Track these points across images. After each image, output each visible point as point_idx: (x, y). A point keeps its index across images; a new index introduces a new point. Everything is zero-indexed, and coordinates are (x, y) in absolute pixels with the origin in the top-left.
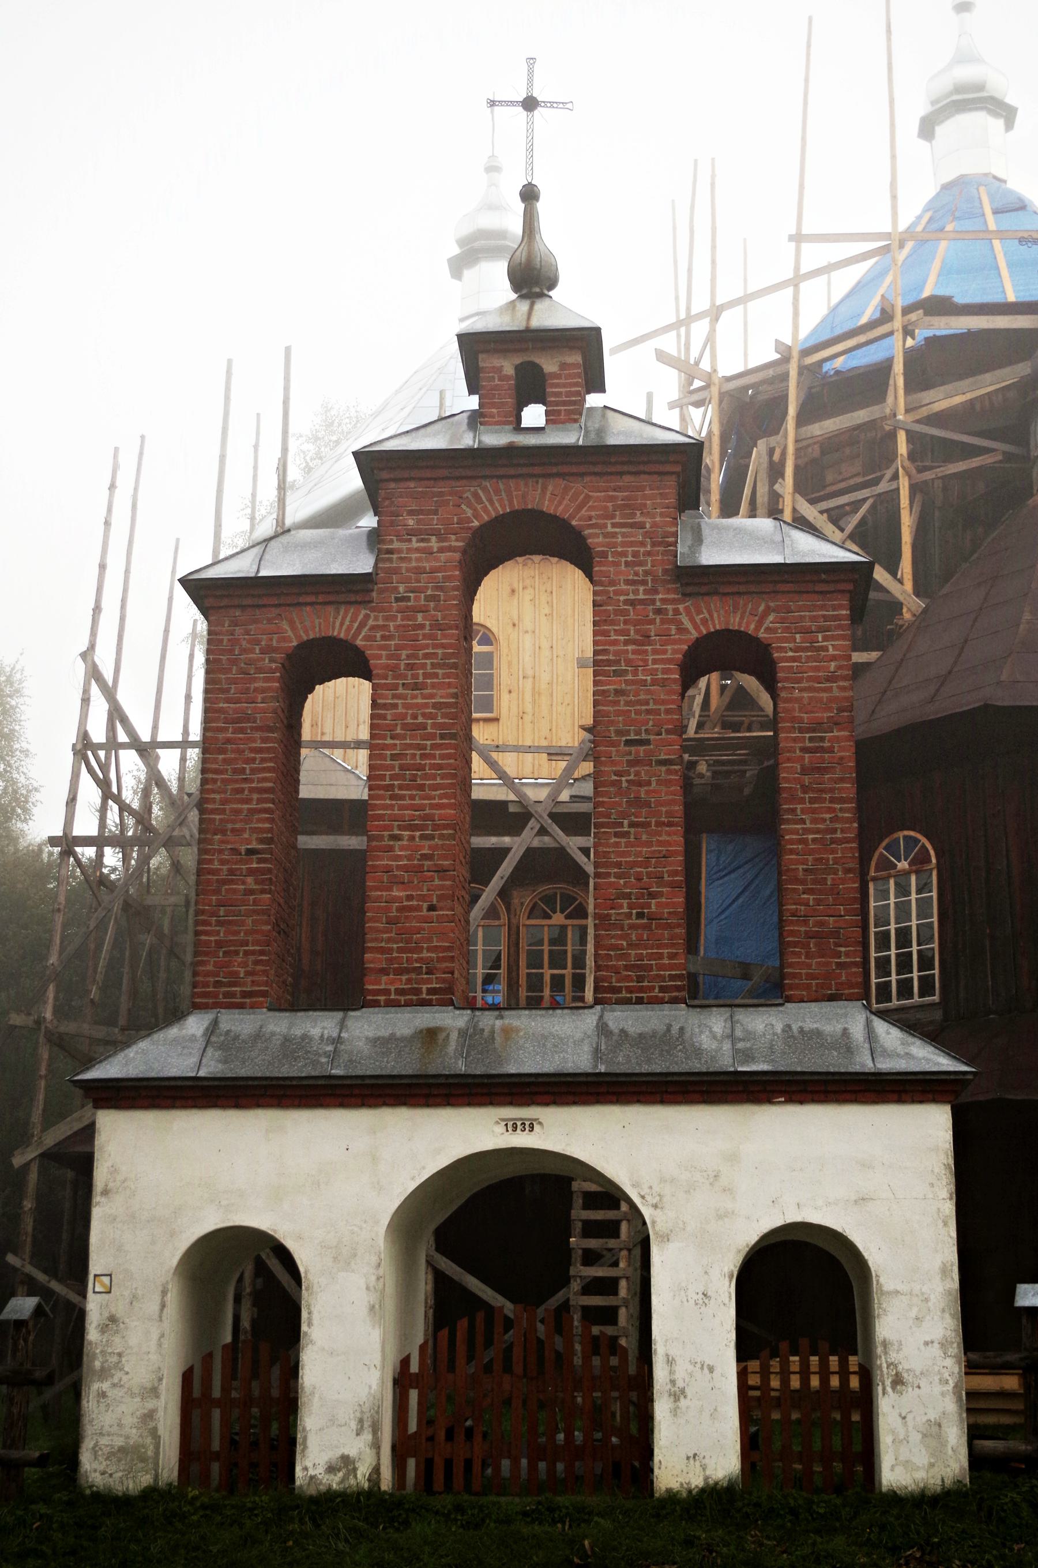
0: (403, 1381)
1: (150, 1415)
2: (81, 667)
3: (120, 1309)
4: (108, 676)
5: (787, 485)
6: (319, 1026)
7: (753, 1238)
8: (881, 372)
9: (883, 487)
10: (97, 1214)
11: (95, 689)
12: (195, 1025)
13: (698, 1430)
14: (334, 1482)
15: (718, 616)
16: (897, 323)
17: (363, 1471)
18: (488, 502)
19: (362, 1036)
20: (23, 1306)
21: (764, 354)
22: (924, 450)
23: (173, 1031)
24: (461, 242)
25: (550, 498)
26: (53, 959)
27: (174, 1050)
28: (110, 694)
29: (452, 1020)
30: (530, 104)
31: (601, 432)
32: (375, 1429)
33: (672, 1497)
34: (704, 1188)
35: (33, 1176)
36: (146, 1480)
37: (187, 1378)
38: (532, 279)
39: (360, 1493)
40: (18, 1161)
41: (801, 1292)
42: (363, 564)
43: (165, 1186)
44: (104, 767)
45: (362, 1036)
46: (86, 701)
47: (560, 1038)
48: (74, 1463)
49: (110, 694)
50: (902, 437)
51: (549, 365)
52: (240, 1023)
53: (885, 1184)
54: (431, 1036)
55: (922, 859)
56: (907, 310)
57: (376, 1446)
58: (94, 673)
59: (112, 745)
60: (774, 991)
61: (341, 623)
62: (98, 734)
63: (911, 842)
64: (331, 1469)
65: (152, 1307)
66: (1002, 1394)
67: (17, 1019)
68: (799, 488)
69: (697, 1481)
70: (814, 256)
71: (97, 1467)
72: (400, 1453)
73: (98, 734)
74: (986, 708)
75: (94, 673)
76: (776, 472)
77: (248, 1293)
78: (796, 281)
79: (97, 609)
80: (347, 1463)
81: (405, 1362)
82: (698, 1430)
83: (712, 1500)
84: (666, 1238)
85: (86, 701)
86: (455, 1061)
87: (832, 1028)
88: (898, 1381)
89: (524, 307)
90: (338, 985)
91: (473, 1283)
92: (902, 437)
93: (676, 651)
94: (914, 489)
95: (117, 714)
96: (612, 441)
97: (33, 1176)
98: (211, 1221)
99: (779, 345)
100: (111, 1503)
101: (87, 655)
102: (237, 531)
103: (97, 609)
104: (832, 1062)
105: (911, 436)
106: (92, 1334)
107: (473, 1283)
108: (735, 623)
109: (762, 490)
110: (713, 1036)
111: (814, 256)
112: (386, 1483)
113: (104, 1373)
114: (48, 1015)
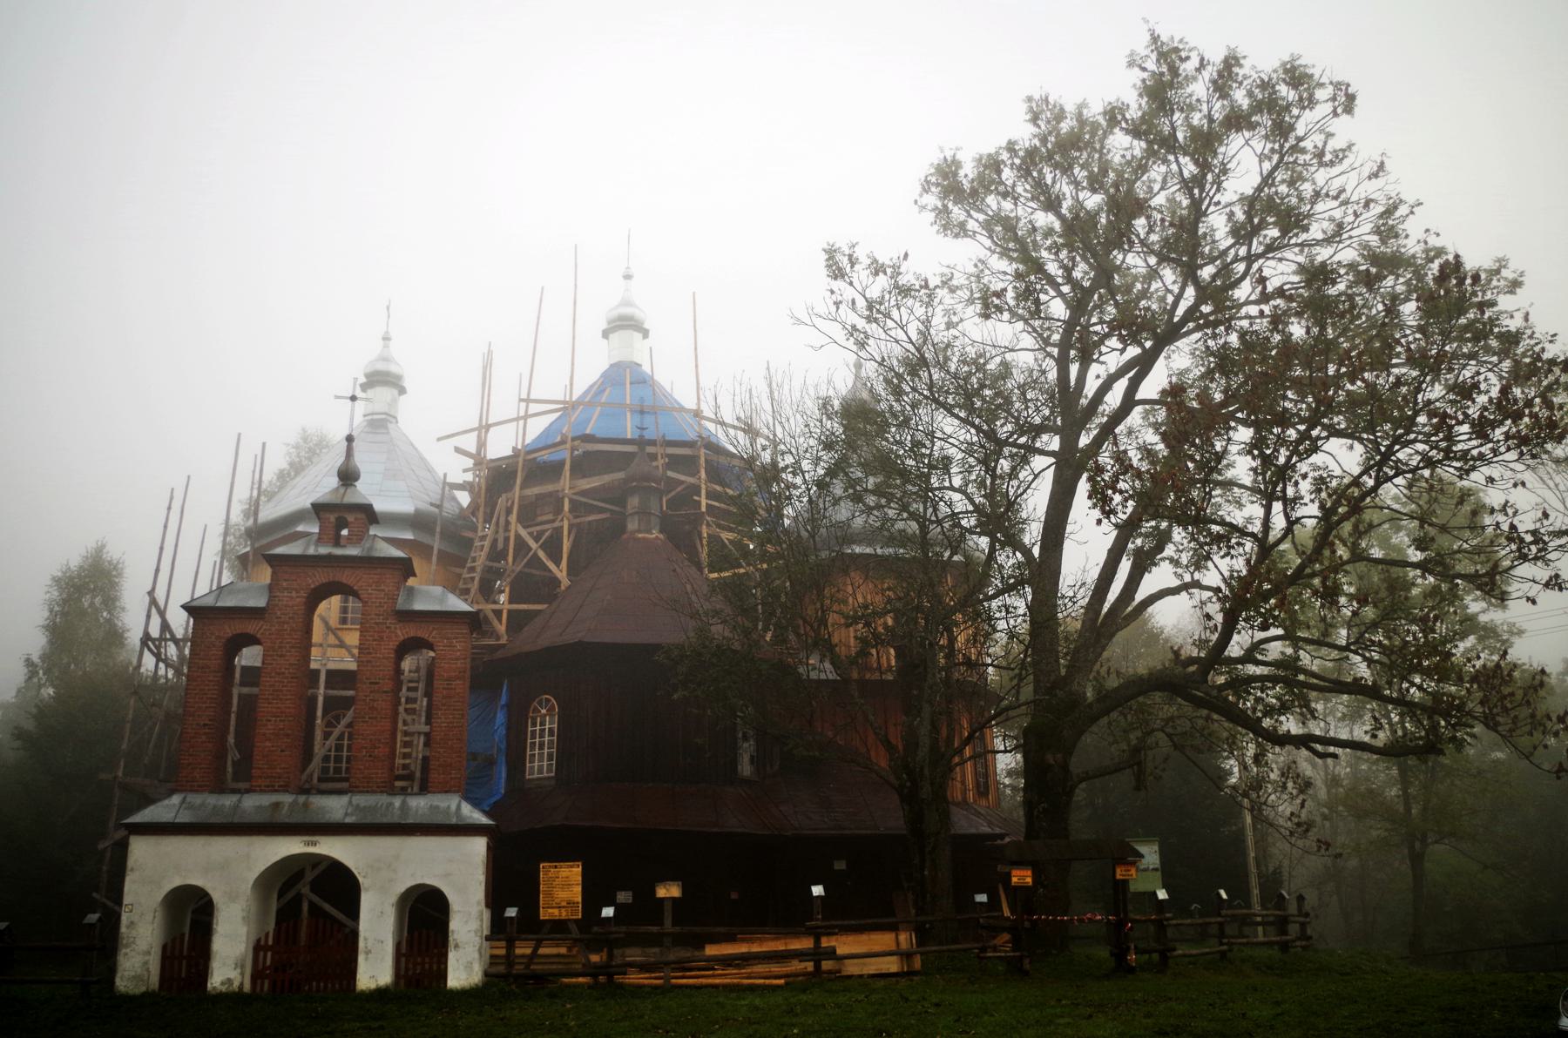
0: (258, 948)
1: (146, 963)
2: (147, 599)
3: (135, 918)
4: (162, 604)
5: (513, 518)
6: (228, 801)
7: (403, 890)
8: (562, 464)
9: (557, 524)
10: (128, 879)
11: (154, 610)
12: (176, 799)
13: (375, 969)
14: (224, 989)
15: (411, 631)
16: (568, 446)
17: (236, 984)
18: (319, 577)
19: (253, 804)
20: (93, 918)
21: (507, 452)
22: (576, 507)
23: (166, 802)
24: (367, 376)
25: (346, 577)
26: (124, 746)
27: (166, 809)
28: (162, 614)
29: (287, 799)
30: (353, 398)
31: (371, 549)
32: (243, 967)
33: (362, 992)
34: (384, 871)
35: (108, 855)
36: (143, 989)
37: (164, 948)
38: (348, 476)
39: (234, 993)
40: (101, 846)
41: (424, 914)
42: (260, 602)
43: (155, 868)
44: (158, 648)
45: (253, 804)
46: (149, 616)
47: (335, 807)
48: (113, 983)
49: (162, 614)
50: (566, 501)
51: (350, 518)
52: (196, 799)
53: (459, 869)
54: (277, 805)
55: (550, 710)
56: (573, 439)
57: (242, 974)
58: (153, 602)
59: (162, 639)
60: (424, 789)
61: (251, 627)
62: (155, 632)
63: (548, 701)
64: (223, 983)
65: (149, 917)
66: (558, 956)
67: (103, 776)
68: (519, 520)
69: (373, 986)
70: (534, 408)
71: (123, 984)
72: (255, 977)
73: (155, 632)
74: (580, 643)
75: (153, 602)
76: (509, 511)
77: (191, 913)
78: (526, 417)
79: (157, 570)
80: (229, 981)
81: (259, 941)
82: (375, 969)
83: (380, 994)
84: (367, 890)
85: (149, 616)
86: (284, 816)
87: (443, 805)
88: (456, 946)
89: (342, 490)
90: (244, 777)
91: (327, 907)
92: (566, 501)
93: (393, 644)
94: (571, 526)
95: (165, 626)
96: (377, 554)
97: (108, 855)
98: (178, 882)
99: (514, 449)
100: (128, 999)
101: (151, 593)
102: (203, 589)
103: (157, 570)
104: (439, 819)
105: (571, 501)
106: (123, 929)
107: (327, 907)
108: (419, 634)
109: (502, 520)
110: (393, 806)
111: (534, 408)
112: (247, 987)
113: (127, 946)
114: (120, 774)
